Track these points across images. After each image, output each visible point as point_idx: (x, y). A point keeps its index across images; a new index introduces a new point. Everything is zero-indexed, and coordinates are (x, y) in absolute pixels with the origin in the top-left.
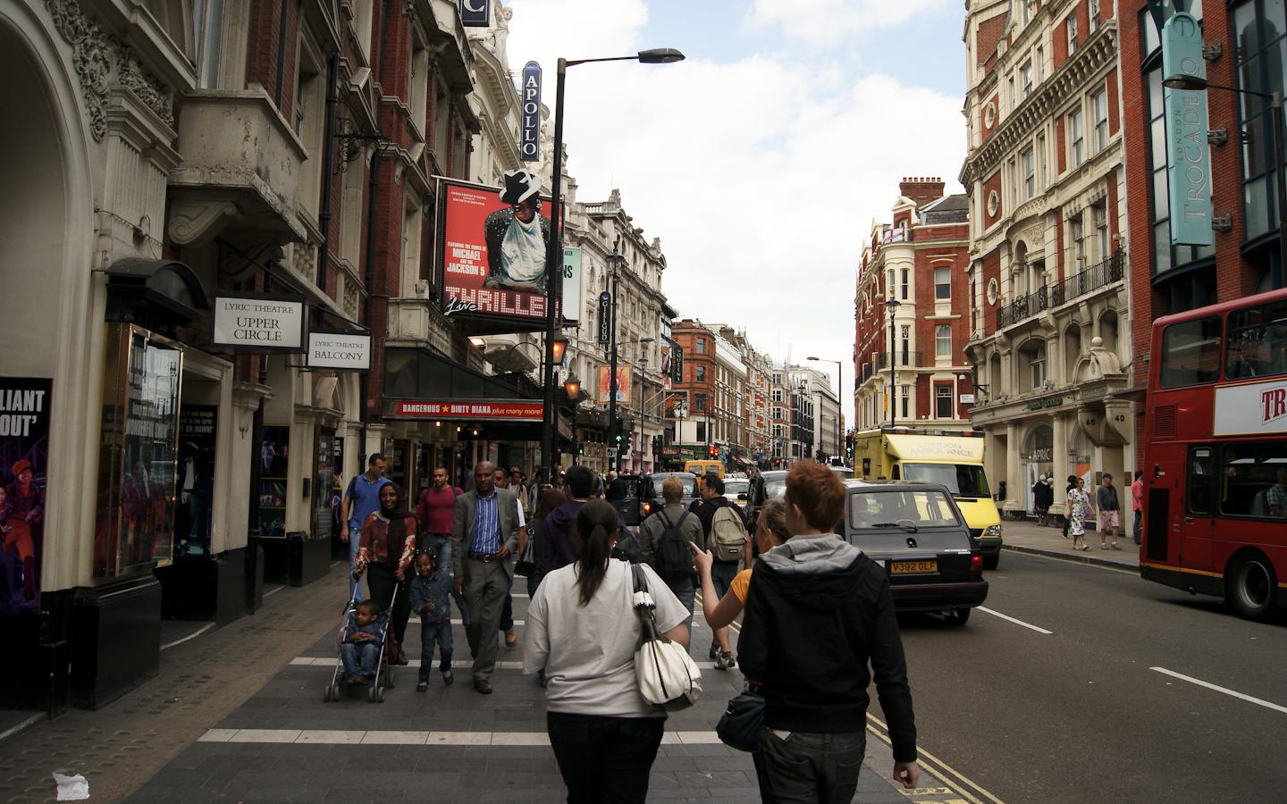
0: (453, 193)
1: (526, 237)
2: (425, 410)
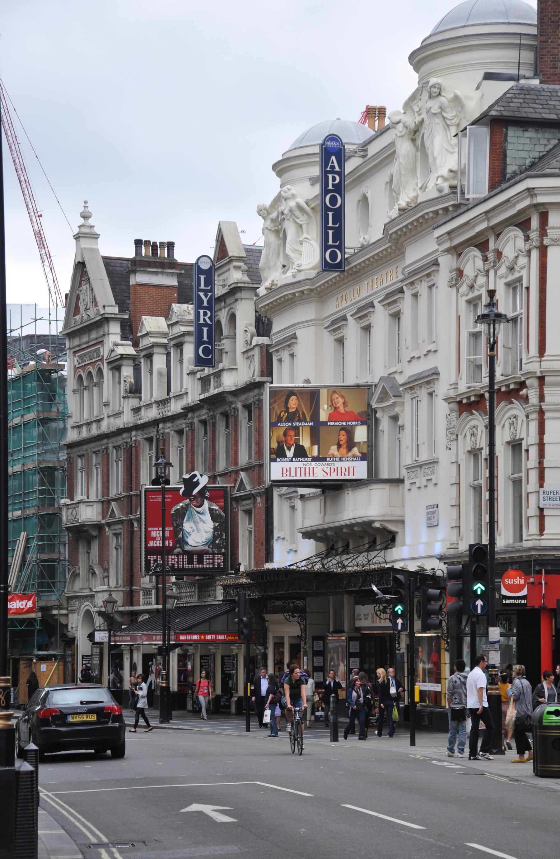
0: (150, 496)
1: (200, 518)
2: (192, 638)
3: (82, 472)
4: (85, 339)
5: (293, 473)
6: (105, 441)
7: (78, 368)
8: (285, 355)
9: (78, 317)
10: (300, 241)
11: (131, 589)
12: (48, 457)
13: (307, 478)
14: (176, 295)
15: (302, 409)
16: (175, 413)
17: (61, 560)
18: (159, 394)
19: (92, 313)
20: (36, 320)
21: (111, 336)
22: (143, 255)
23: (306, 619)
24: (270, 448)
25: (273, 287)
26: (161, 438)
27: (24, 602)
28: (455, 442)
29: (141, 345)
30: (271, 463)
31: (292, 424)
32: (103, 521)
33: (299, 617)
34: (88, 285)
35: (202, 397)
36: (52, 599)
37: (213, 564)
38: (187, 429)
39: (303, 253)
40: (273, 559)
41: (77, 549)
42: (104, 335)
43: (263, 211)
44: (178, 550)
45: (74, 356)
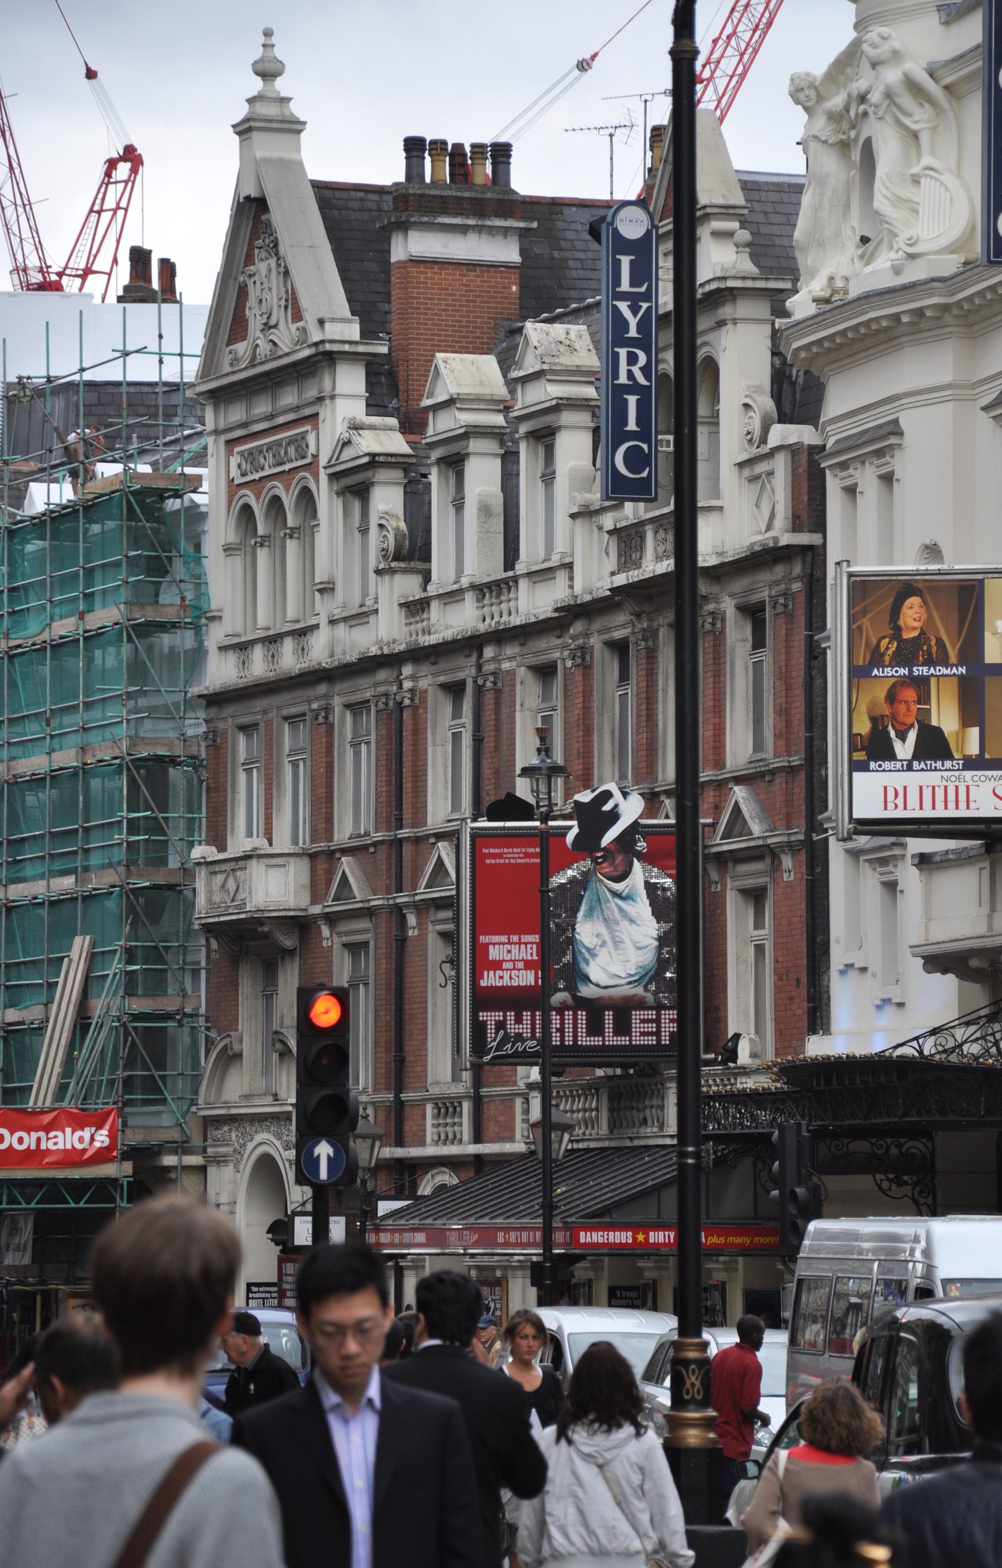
1: (621, 910)
2: (611, 1240)
3: (249, 772)
4: (262, 407)
5: (913, 800)
6: (322, 689)
7: (241, 485)
8: (867, 478)
9: (241, 348)
10: (913, 175)
11: (397, 1097)
12: (149, 729)
13: (952, 813)
14: (514, 288)
15: (937, 630)
16: (533, 620)
17: (185, 1015)
18: (481, 563)
19: (285, 336)
20: (126, 354)
21: (339, 402)
22: (428, 179)
23: (933, 1191)
24: (851, 736)
25: (836, 297)
26: (489, 684)
27: (86, 1133)
28: (79, 281)
29: (430, 431)
30: (855, 775)
31: (911, 671)
32: (316, 910)
33: (915, 1184)
34: (273, 261)
35: (621, 580)
36: (157, 1124)
37: (658, 1034)
38: (569, 664)
39: (920, 208)
40: (828, 1024)
41: (235, 984)
42: (320, 399)
43: (807, 92)
44: (559, 997)
45: (229, 453)
